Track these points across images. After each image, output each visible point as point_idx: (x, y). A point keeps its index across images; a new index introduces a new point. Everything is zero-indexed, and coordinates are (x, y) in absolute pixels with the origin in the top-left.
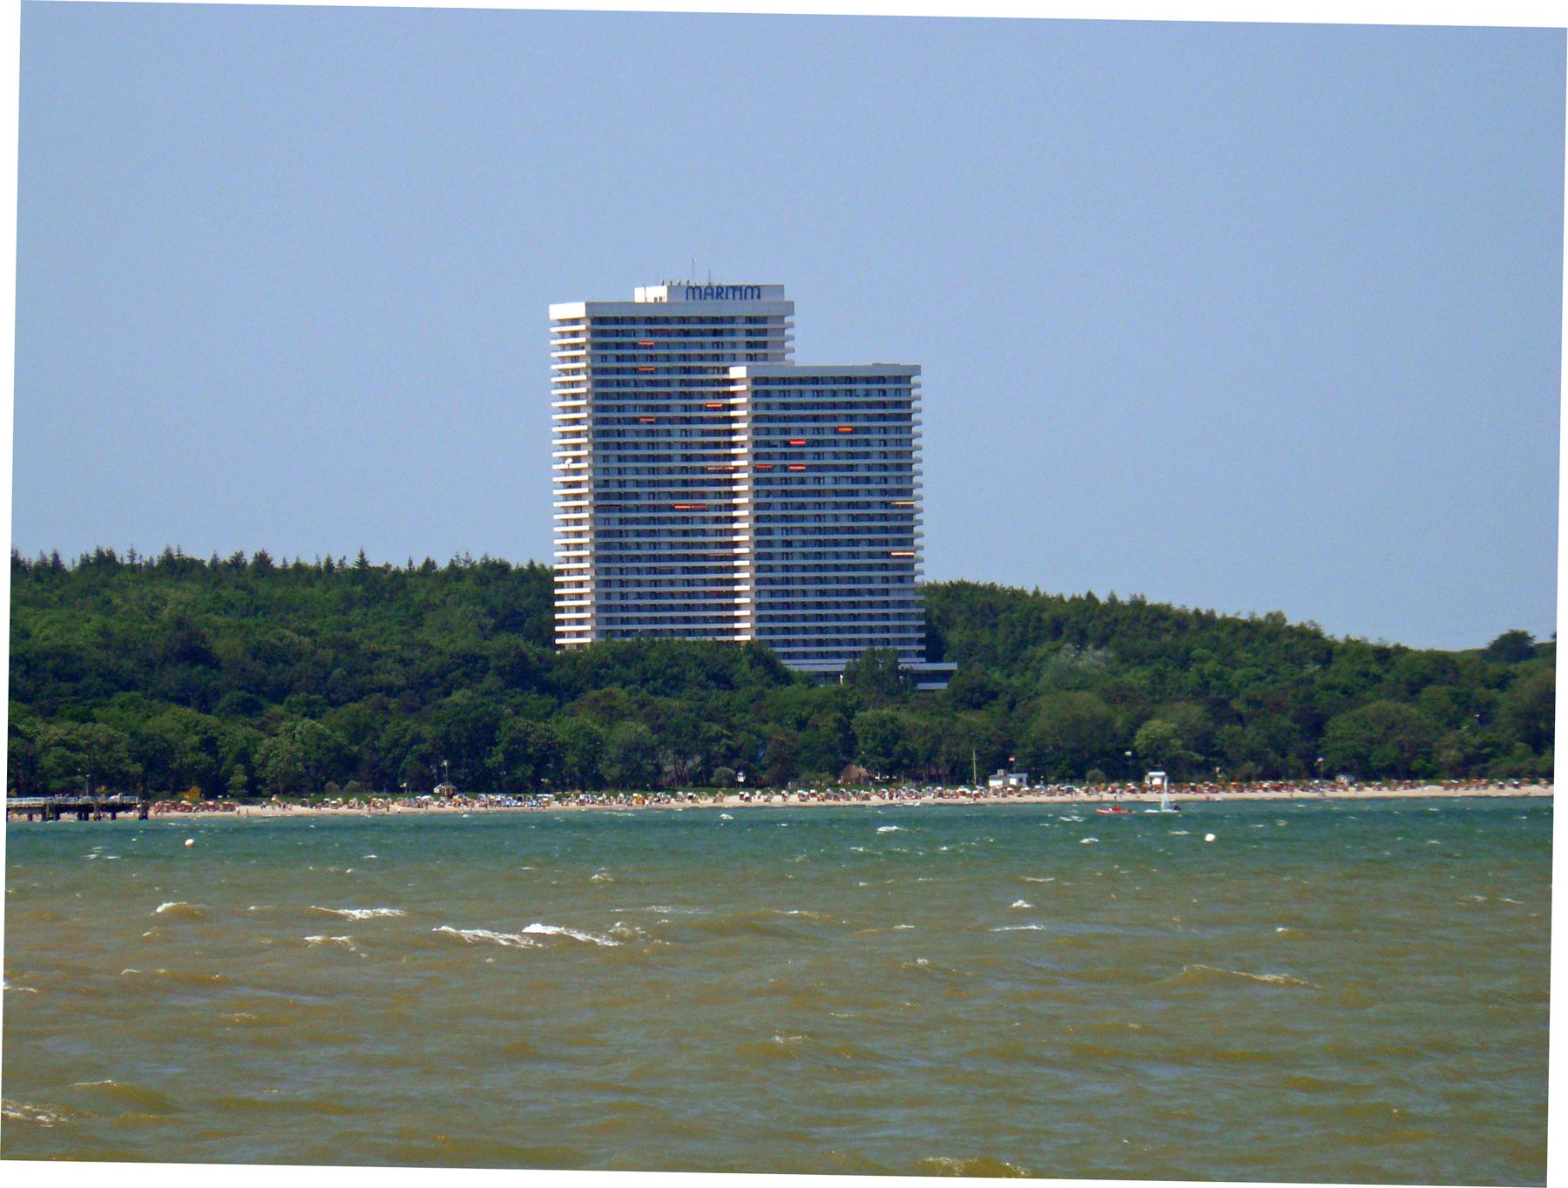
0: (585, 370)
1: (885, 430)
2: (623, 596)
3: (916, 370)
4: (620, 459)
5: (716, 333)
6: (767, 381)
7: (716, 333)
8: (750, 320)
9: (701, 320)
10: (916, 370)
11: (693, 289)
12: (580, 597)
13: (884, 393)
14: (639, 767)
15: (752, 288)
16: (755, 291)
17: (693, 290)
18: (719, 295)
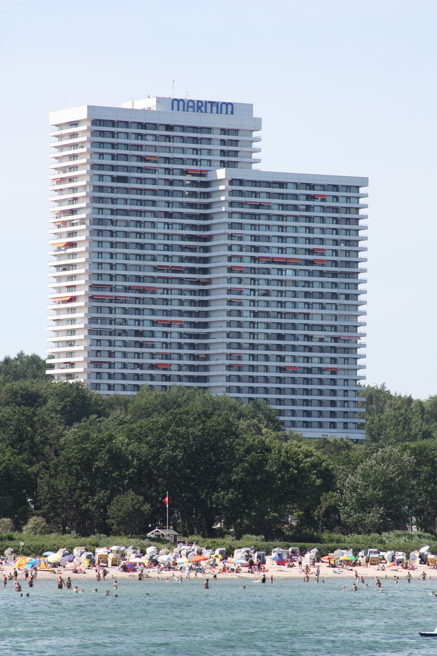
0: (82, 221)
1: (336, 285)
2: (310, 230)
3: (365, 182)
5: (196, 140)
6: (241, 182)
7: (196, 140)
8: (224, 131)
9: (184, 128)
10: (365, 182)
11: (178, 101)
12: (73, 321)
13: (337, 198)
15: (227, 104)
16: (227, 108)
17: (177, 104)
18: (199, 108)
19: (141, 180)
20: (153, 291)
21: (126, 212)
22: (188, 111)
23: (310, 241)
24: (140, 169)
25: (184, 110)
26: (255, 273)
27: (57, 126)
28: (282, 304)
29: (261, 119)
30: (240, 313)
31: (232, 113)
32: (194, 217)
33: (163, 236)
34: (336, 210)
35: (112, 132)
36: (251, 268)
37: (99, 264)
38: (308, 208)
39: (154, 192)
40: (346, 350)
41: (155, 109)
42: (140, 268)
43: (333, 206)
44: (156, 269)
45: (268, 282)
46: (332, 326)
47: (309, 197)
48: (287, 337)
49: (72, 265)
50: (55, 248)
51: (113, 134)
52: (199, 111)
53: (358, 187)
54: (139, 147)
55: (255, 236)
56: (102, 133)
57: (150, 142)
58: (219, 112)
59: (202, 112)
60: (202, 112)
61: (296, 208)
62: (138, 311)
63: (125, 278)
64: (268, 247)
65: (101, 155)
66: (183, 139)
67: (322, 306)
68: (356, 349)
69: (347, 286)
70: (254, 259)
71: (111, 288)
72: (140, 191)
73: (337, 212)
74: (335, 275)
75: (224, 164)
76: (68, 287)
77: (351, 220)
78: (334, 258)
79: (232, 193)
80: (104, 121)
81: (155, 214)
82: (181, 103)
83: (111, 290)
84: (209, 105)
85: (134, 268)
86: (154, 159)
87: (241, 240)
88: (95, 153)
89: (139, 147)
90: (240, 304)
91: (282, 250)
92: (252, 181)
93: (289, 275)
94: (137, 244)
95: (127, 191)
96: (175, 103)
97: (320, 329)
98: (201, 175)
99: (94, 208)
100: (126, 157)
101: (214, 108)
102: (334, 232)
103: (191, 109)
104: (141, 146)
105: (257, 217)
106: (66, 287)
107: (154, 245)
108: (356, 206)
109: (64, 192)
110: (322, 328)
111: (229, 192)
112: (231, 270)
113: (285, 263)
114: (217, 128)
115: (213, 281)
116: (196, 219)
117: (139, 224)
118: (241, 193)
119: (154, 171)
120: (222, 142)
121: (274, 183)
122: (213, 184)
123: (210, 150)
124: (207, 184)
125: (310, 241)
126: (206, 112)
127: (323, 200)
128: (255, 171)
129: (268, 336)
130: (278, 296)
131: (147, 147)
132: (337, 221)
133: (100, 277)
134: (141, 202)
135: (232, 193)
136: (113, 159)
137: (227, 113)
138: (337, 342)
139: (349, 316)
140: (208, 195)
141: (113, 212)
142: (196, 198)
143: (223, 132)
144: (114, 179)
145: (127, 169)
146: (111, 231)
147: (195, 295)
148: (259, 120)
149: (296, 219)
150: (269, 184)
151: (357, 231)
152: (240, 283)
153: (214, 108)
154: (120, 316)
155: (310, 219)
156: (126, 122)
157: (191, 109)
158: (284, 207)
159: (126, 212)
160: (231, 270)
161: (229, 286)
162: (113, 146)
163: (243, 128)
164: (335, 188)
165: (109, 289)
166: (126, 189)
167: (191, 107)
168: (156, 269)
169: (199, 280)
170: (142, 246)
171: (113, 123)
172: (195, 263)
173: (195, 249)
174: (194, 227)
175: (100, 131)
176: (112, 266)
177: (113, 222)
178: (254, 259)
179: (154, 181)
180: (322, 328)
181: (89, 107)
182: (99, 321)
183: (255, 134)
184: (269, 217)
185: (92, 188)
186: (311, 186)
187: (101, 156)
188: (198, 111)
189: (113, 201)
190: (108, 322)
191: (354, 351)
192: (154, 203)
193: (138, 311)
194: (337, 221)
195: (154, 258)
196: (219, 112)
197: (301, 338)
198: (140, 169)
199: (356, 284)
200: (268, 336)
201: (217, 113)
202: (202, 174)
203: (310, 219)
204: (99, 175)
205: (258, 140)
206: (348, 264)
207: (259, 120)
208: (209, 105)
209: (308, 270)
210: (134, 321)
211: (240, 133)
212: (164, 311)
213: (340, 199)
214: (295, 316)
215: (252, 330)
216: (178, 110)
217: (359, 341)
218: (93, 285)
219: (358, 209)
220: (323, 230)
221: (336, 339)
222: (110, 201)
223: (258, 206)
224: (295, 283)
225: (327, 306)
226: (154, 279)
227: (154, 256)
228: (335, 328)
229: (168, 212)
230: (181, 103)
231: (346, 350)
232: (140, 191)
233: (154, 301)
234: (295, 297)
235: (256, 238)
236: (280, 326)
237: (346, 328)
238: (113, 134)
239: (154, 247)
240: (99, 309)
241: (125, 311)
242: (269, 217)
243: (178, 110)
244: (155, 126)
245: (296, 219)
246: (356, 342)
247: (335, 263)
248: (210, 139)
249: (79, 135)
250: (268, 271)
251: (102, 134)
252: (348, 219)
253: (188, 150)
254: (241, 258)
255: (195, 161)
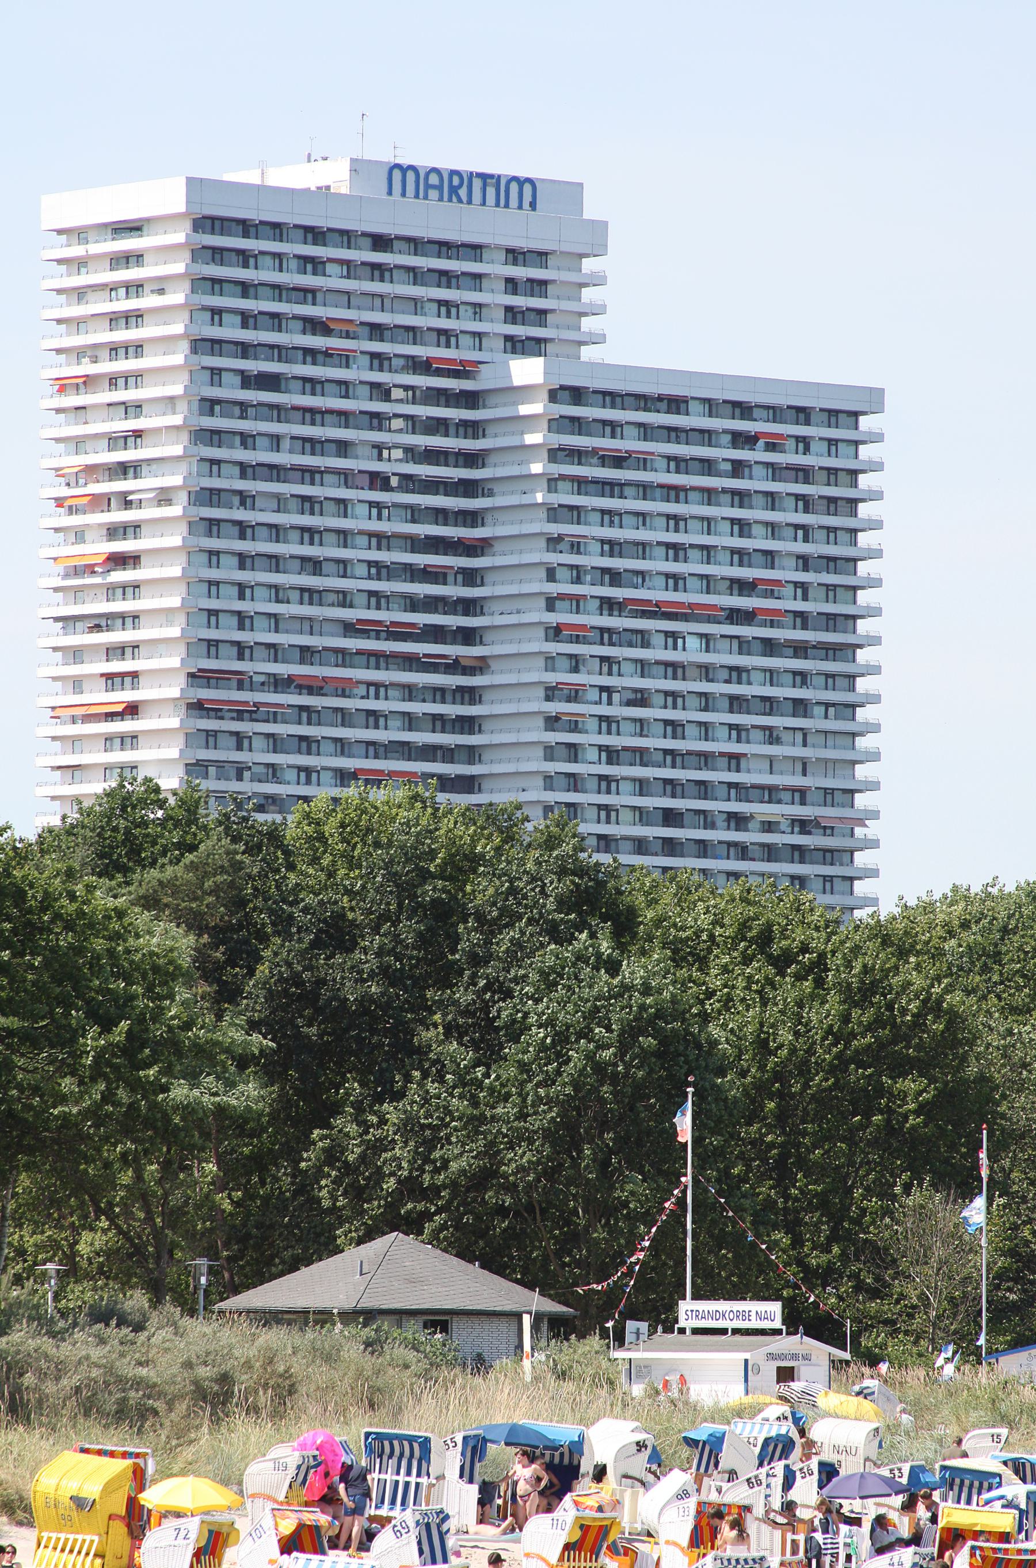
0: (164, 497)
2: (742, 527)
3: (874, 399)
4: (243, 560)
5: (445, 278)
6: (577, 394)
7: (445, 278)
8: (514, 255)
9: (416, 245)
10: (874, 399)
11: (404, 169)
13: (804, 443)
14: (542, 1047)
15: (521, 182)
16: (517, 191)
17: (402, 177)
19: (312, 384)
20: (343, 690)
21: (275, 472)
22: (426, 197)
23: (741, 556)
24: (311, 354)
25: (417, 196)
26: (611, 644)
27: (60, 232)
28: (674, 728)
29: (606, 223)
30: (573, 752)
31: (533, 205)
32: (441, 489)
33: (366, 538)
34: (804, 474)
35: (241, 252)
36: (602, 630)
37: (212, 613)
38: (738, 468)
39: (344, 417)
40: (828, 855)
41: (345, 190)
42: (310, 625)
43: (787, 465)
44: (349, 628)
45: (643, 667)
46: (793, 790)
47: (741, 439)
48: (687, 819)
49: (123, 616)
50: (60, 568)
51: (244, 257)
52: (454, 199)
53: (855, 414)
54: (308, 294)
55: (611, 543)
56: (217, 254)
57: (334, 280)
58: (502, 202)
59: (460, 201)
60: (460, 201)
61: (708, 466)
62: (306, 744)
63: (274, 651)
64: (642, 574)
65: (216, 313)
66: (415, 275)
67: (772, 736)
68: (852, 853)
69: (830, 681)
70: (609, 605)
71: (242, 682)
72: (311, 415)
73: (806, 481)
74: (800, 650)
75: (516, 346)
76: (109, 677)
77: (839, 503)
78: (800, 606)
79: (557, 424)
80: (223, 219)
81: (346, 477)
82: (411, 176)
83: (240, 687)
84: (477, 184)
85: (297, 625)
86: (344, 327)
87: (579, 553)
88: (204, 308)
89: (308, 294)
90: (574, 727)
91: (675, 580)
92: (605, 393)
93: (693, 652)
94: (304, 559)
95: (278, 412)
96: (397, 175)
97: (766, 798)
98: (456, 374)
99: (202, 460)
100: (276, 320)
101: (491, 191)
102: (800, 533)
103: (433, 194)
104: (313, 291)
105: (616, 489)
106: (102, 675)
107: (343, 562)
108: (852, 465)
109: (90, 414)
110: (770, 793)
111: (550, 420)
112: (556, 632)
113: (685, 618)
114: (498, 247)
115: (494, 665)
116: (446, 495)
117: (308, 504)
118: (577, 425)
119: (345, 359)
120: (510, 286)
121: (660, 398)
122: (491, 400)
123: (480, 305)
124: (471, 399)
125: (741, 556)
126: (470, 202)
127: (771, 447)
128: (592, 365)
129: (642, 815)
130: (666, 707)
131: (328, 296)
132: (806, 503)
133: (213, 649)
134: (312, 445)
135: (557, 424)
136: (245, 325)
137: (520, 207)
138: (809, 833)
139: (835, 761)
140: (473, 429)
141: (245, 470)
142: (447, 435)
143: (510, 256)
144: (248, 381)
145: (279, 352)
146: (239, 523)
147: (443, 702)
148: (600, 228)
149: (709, 495)
150: (644, 401)
151: (854, 531)
152: (575, 670)
153: (491, 191)
154: (260, 756)
155: (741, 497)
156: (276, 226)
157: (433, 194)
158: (679, 464)
159: (275, 472)
160: (556, 632)
161: (552, 678)
162: (246, 289)
163: (565, 247)
164: (802, 416)
165: (234, 683)
166: (277, 407)
167: (434, 187)
168: (349, 628)
169: (456, 661)
170: (315, 565)
171: (246, 227)
172: (445, 613)
173: (445, 575)
174: (441, 515)
175: (214, 249)
176: (243, 620)
177: (245, 499)
178: (609, 605)
179: (345, 388)
180: (770, 793)
181: (190, 181)
182: (212, 770)
183: (588, 265)
184: (645, 490)
185: (196, 405)
186: (743, 409)
187: (216, 318)
188: (450, 200)
189: (247, 440)
190: (233, 773)
191: (846, 857)
192: (343, 448)
193: (306, 744)
194: (806, 503)
195: (344, 599)
196: (502, 202)
197: (720, 821)
198: (311, 354)
199: (852, 678)
200: (642, 815)
201: (497, 205)
202: (462, 371)
203: (741, 497)
204: (212, 369)
205: (598, 280)
206: (831, 621)
207: (600, 228)
208: (477, 184)
209: (737, 637)
210: (296, 771)
211: (552, 261)
212: (369, 743)
213: (813, 446)
214: (705, 759)
215: (604, 799)
216: (404, 194)
217: (859, 831)
218: (200, 670)
219: (854, 473)
220: (773, 529)
221: (803, 826)
222: (237, 440)
223: (618, 461)
224: (706, 672)
225: (786, 737)
226: (343, 657)
227: (344, 593)
228: (801, 795)
229: (378, 473)
230: (411, 176)
231: (829, 855)
232: (311, 415)
233: (344, 718)
234: (706, 709)
235: (613, 547)
236: (671, 787)
237: (828, 795)
238: (244, 257)
239: (343, 567)
240: (210, 737)
241: (275, 743)
242: (645, 490)
243: (404, 194)
244: (347, 237)
245: (709, 495)
246: (852, 835)
247: (802, 619)
248: (478, 277)
249: (146, 258)
250: (643, 639)
251: (218, 257)
252: (832, 500)
253: (428, 305)
254: (577, 602)
255: (445, 336)
